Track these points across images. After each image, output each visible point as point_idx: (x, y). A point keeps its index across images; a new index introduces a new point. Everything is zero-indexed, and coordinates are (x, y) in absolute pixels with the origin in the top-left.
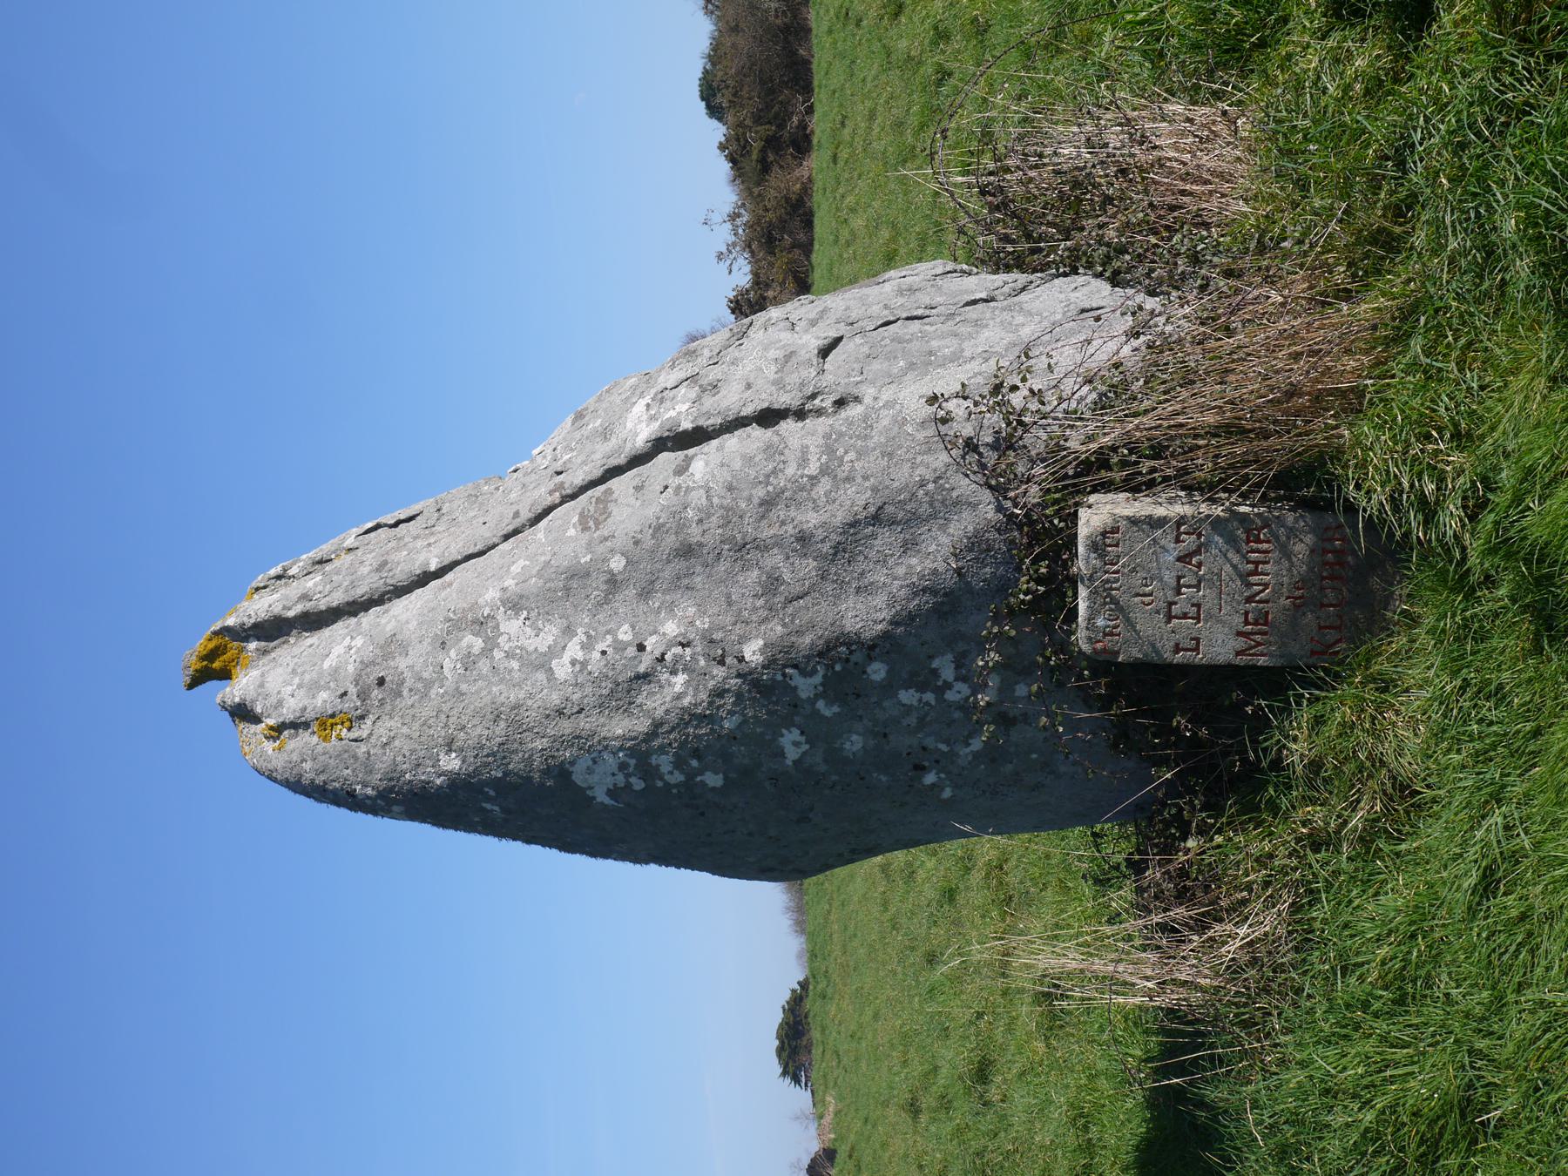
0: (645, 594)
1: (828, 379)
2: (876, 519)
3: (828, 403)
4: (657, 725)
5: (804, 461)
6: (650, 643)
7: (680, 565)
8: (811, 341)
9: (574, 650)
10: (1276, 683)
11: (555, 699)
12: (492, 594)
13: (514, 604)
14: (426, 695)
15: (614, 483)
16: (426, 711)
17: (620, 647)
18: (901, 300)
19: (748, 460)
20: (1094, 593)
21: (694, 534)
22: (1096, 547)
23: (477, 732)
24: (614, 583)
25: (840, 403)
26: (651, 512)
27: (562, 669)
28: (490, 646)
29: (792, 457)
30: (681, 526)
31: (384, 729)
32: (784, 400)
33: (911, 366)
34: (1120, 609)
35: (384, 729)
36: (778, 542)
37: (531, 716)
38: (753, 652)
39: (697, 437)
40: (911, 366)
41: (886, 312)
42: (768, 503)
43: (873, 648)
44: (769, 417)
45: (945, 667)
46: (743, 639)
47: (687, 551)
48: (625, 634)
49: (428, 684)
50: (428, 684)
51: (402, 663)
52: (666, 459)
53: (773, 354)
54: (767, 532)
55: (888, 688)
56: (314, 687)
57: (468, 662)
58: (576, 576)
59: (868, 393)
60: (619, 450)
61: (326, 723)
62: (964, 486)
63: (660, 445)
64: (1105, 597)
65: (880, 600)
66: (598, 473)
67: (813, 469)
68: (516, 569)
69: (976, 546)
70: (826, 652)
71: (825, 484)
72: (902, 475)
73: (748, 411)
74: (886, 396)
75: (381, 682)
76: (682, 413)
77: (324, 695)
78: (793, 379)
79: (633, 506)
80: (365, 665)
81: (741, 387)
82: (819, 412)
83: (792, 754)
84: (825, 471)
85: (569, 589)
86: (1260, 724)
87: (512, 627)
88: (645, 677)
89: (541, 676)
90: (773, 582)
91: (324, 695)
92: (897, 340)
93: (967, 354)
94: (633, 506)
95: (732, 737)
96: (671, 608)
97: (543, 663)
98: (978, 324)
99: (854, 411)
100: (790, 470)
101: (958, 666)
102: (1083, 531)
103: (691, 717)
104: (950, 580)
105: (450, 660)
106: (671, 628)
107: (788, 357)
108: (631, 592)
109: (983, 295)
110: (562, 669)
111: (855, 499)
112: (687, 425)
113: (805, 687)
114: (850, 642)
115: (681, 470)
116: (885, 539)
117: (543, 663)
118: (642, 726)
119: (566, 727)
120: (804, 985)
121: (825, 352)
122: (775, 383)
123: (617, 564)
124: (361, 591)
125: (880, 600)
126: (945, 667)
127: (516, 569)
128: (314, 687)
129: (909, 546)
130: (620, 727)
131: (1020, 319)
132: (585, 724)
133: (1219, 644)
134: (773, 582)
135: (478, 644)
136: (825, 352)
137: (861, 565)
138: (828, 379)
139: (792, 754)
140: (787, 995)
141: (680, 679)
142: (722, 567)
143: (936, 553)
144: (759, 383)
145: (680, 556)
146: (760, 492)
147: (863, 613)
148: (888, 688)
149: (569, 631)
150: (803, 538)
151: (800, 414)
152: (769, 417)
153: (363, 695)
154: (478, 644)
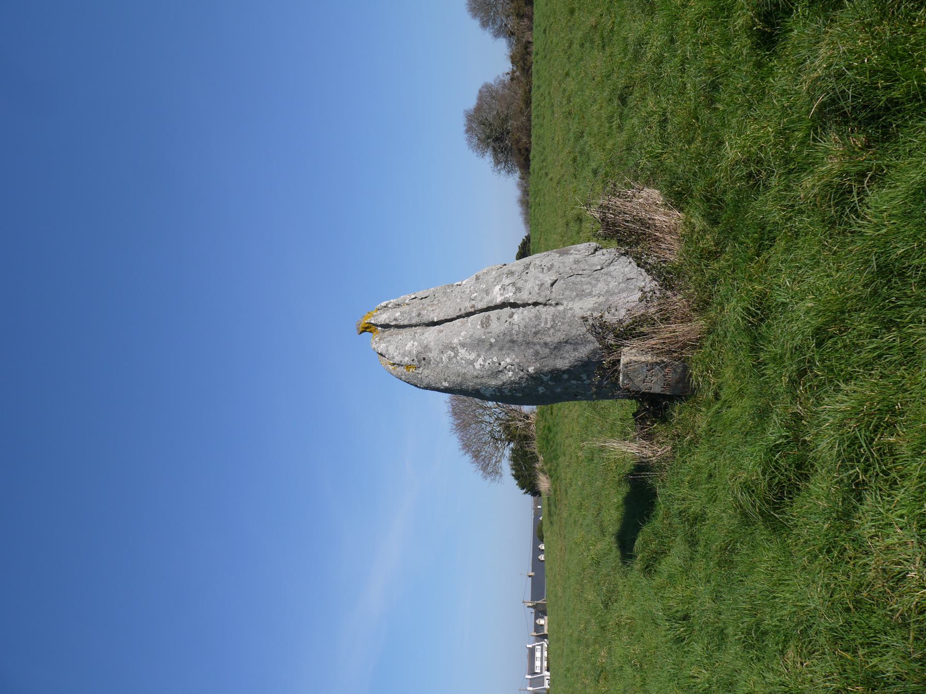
0: (501, 349)
1: (553, 295)
2: (566, 342)
3: (553, 303)
4: (504, 383)
5: (546, 323)
6: (502, 363)
7: (510, 344)
8: (548, 279)
9: (480, 361)
10: (671, 398)
11: (475, 373)
12: (456, 341)
13: (463, 345)
14: (437, 365)
15: (493, 314)
16: (438, 370)
17: (494, 363)
18: (575, 266)
19: (530, 319)
20: (624, 376)
21: (515, 338)
22: (624, 365)
23: (453, 378)
24: (491, 344)
25: (557, 304)
26: (503, 328)
27: (477, 366)
28: (456, 355)
29: (543, 320)
30: (511, 335)
31: (426, 372)
32: (541, 300)
34: (631, 380)
35: (426, 372)
36: (539, 344)
37: (468, 377)
38: (531, 370)
39: (514, 305)
40: (577, 295)
42: (536, 333)
43: (564, 372)
44: (536, 304)
45: (584, 377)
46: (529, 366)
47: (513, 342)
48: (495, 359)
49: (438, 363)
50: (438, 363)
51: (430, 355)
52: (508, 310)
53: (537, 282)
54: (536, 341)
55: (568, 380)
56: (404, 355)
57: (450, 359)
58: (480, 342)
59: (565, 303)
60: (492, 301)
61: (408, 367)
62: (591, 337)
63: (503, 305)
64: (626, 376)
65: (567, 361)
66: (485, 307)
67: (549, 326)
68: (463, 334)
69: (594, 352)
70: (552, 372)
71: (552, 331)
72: (574, 332)
73: (530, 302)
74: (570, 306)
75: (424, 359)
76: (510, 296)
77: (407, 359)
78: (543, 294)
79: (499, 322)
80: (419, 353)
81: (527, 293)
82: (551, 305)
83: (541, 391)
84: (552, 327)
85: (477, 344)
86: (666, 407)
87: (462, 352)
88: (501, 371)
89: (471, 367)
90: (537, 353)
91: (407, 359)
92: (574, 283)
94: (499, 322)
95: (525, 387)
96: (508, 354)
97: (472, 363)
98: (598, 280)
99: (560, 308)
100: (542, 325)
101: (588, 376)
102: (622, 362)
103: (513, 382)
104: (586, 359)
105: (445, 358)
106: (508, 360)
107: (542, 284)
108: (497, 348)
109: (599, 268)
110: (477, 366)
111: (560, 336)
112: (512, 301)
113: (545, 378)
114: (559, 370)
115: (511, 316)
116: (568, 347)
117: (472, 363)
118: (501, 383)
119: (479, 381)
120: (528, 238)
121: (552, 285)
122: (539, 294)
123: (493, 340)
124: (413, 322)
125: (567, 361)
126: (584, 377)
127: (463, 334)
128: (404, 355)
129: (574, 350)
130: (493, 382)
131: (610, 279)
132: (484, 381)
133: (657, 389)
134: (537, 353)
135: (453, 354)
136: (552, 285)
137: (561, 352)
138: (553, 295)
139: (541, 391)
140: (521, 241)
141: (511, 373)
142: (523, 347)
143: (583, 352)
144: (533, 293)
145: (509, 342)
146: (534, 330)
147: (562, 364)
148: (568, 380)
149: (479, 356)
150: (546, 344)
151: (545, 305)
152: (536, 304)
153: (419, 361)
154: (453, 354)
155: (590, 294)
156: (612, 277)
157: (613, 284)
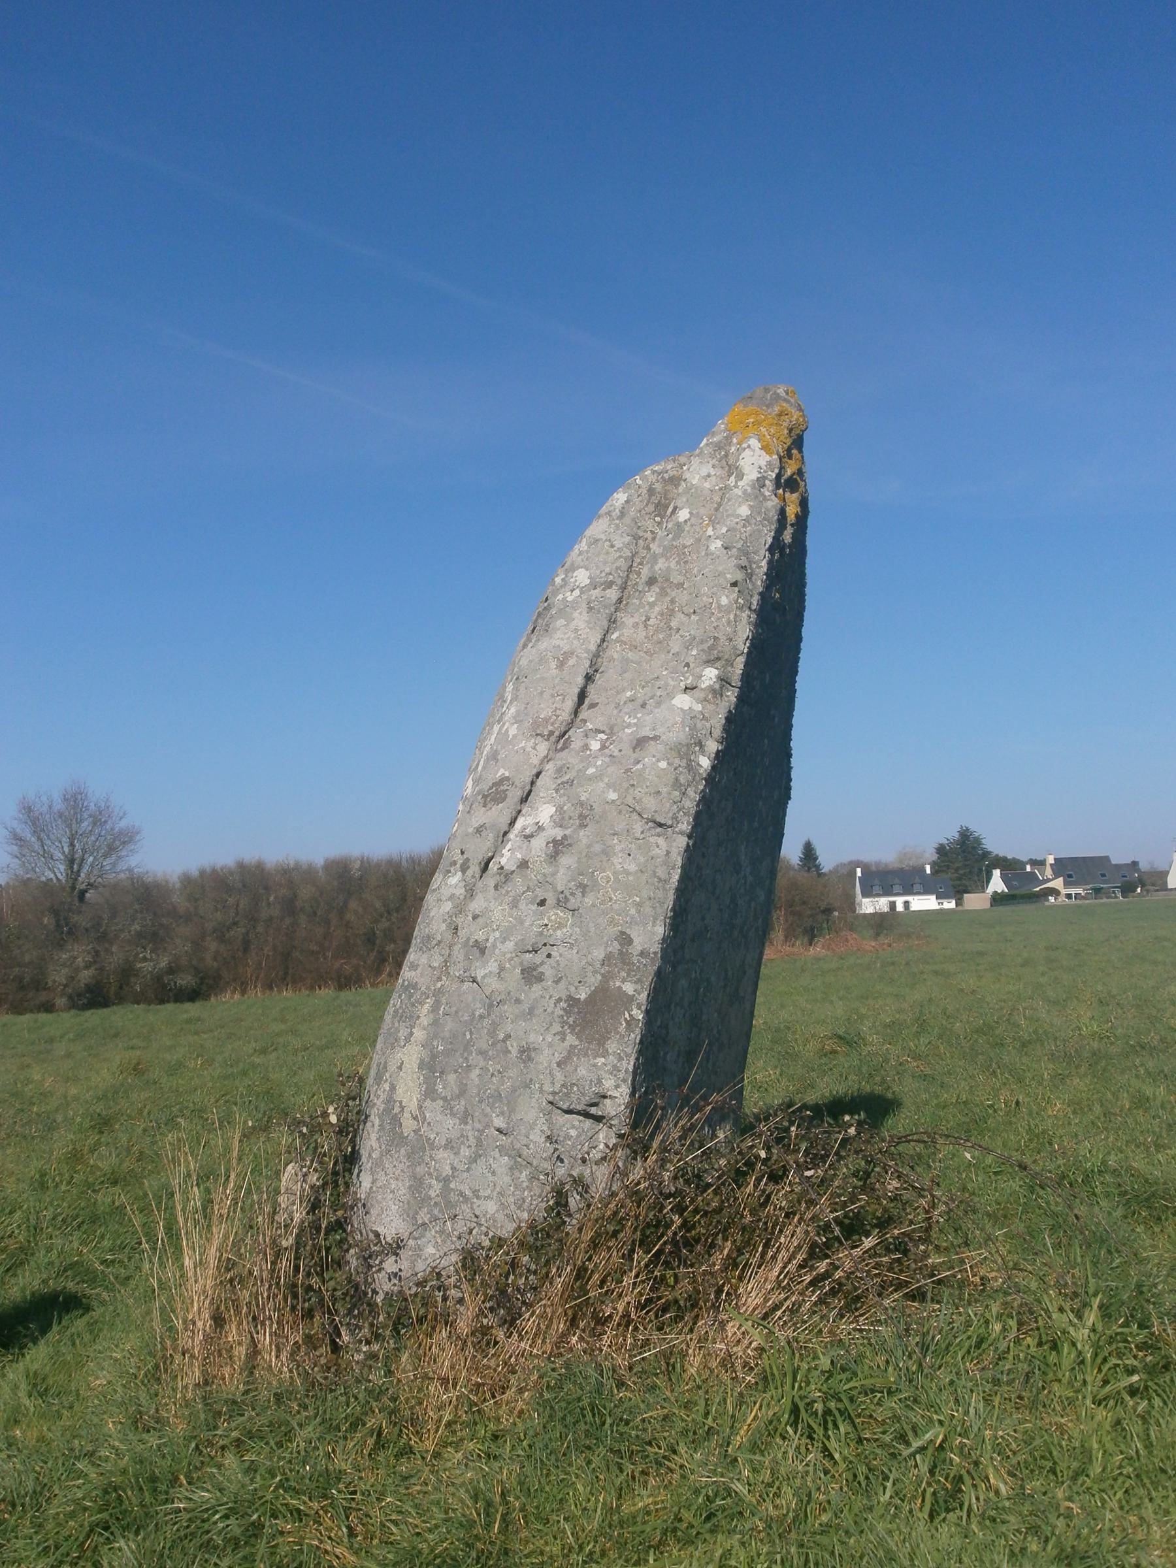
18: (514, 1052)
33: (434, 1056)
41: (502, 1036)
93: (428, 1103)
131: (465, 1152)
155: (430, 1093)
156: (474, 1160)
157: (445, 1161)
